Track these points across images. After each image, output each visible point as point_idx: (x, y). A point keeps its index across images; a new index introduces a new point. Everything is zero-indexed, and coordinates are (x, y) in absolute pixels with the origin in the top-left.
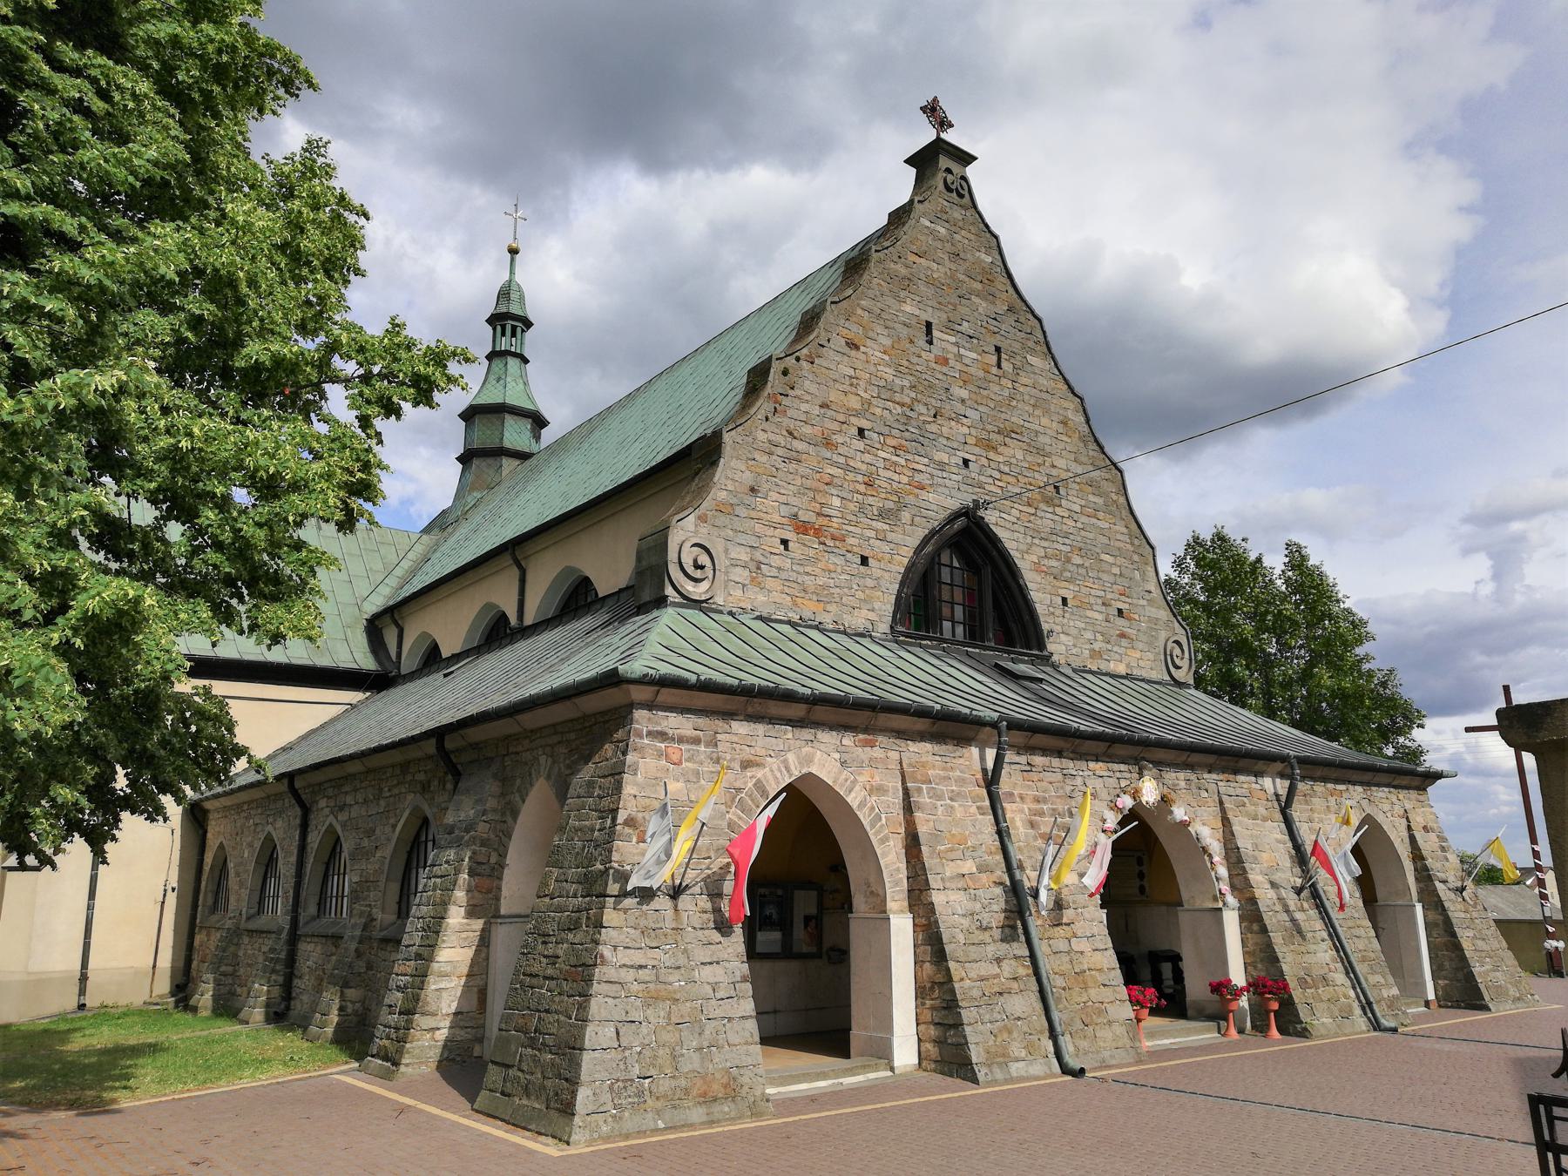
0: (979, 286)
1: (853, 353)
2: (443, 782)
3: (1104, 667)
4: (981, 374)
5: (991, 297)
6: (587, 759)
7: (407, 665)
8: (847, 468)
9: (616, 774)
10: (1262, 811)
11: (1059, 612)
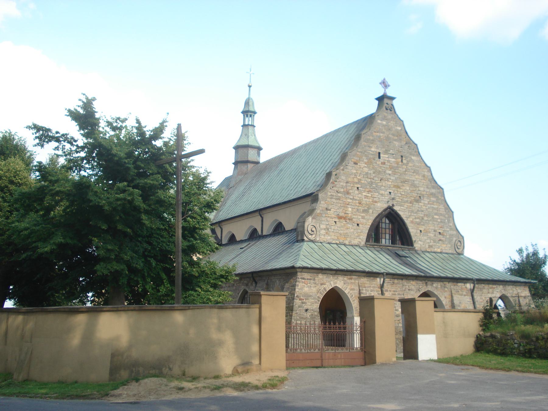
0: (396, 138)
1: (356, 166)
2: (252, 284)
3: (433, 250)
4: (396, 165)
5: (400, 140)
6: (287, 282)
7: (224, 241)
8: (353, 199)
9: (294, 286)
10: (464, 293)
11: (418, 235)
